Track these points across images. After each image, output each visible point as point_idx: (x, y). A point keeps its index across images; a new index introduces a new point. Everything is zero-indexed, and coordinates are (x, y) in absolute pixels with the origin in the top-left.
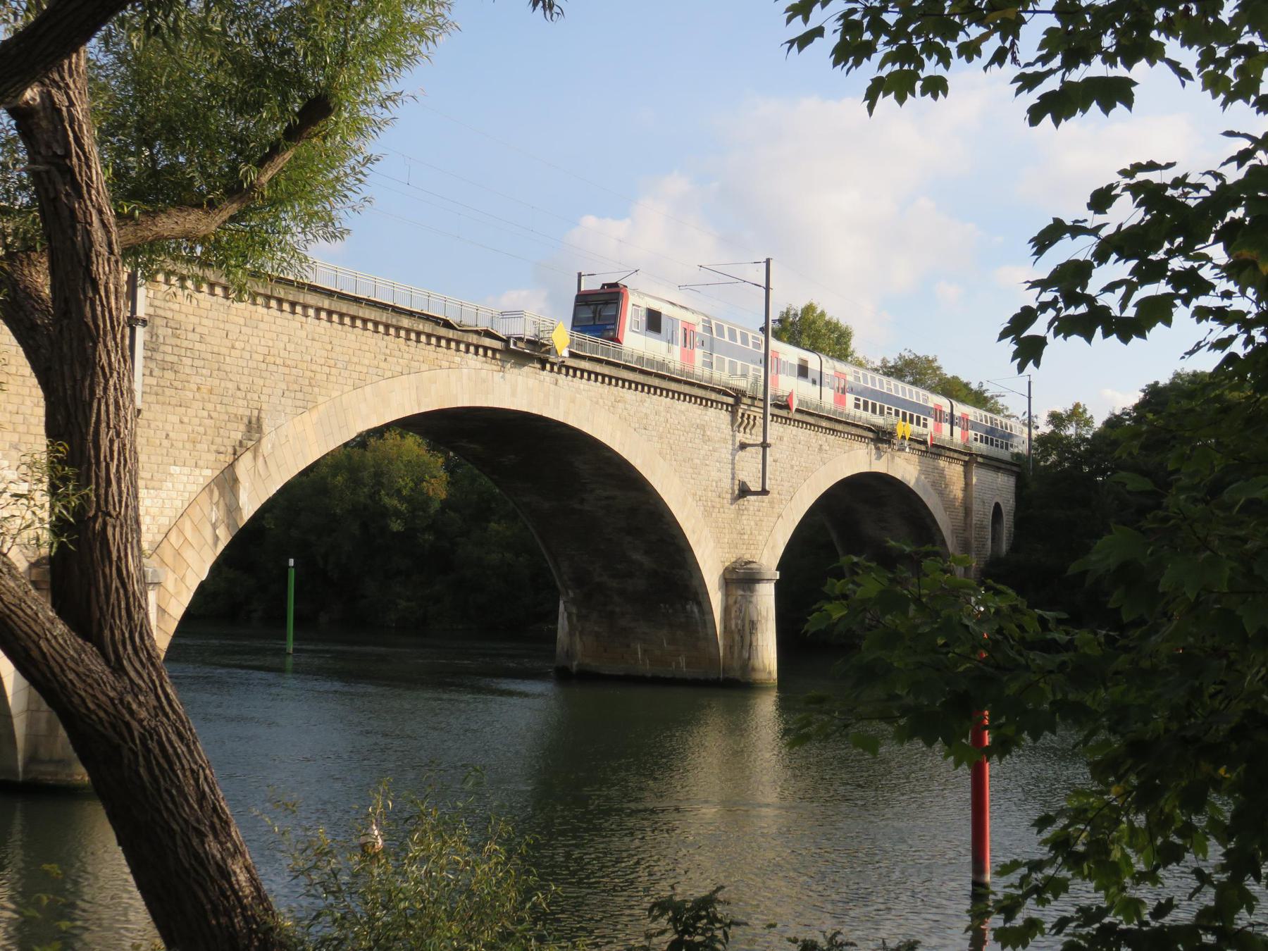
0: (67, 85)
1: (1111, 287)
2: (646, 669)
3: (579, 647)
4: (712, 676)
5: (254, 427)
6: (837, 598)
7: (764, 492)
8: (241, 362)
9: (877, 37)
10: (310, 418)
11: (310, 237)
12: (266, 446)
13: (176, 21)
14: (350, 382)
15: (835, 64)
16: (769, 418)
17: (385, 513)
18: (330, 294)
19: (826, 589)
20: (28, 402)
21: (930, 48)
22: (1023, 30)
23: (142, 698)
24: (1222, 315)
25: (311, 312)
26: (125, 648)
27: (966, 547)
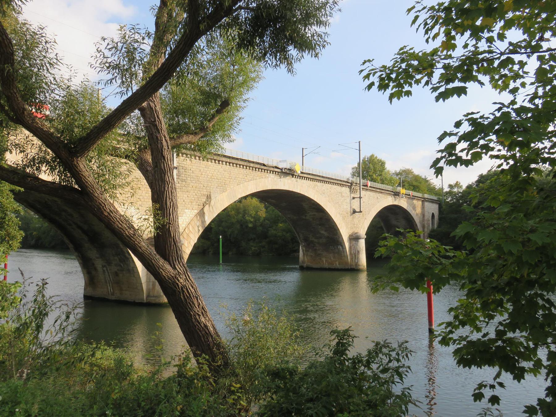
0: (154, 101)
1: (462, 151)
2: (326, 266)
3: (306, 259)
4: (347, 267)
5: (209, 197)
6: (383, 246)
7: (361, 212)
8: (205, 179)
9: (389, 82)
10: (225, 194)
11: (224, 141)
12: (212, 202)
13: (185, 82)
14: (236, 183)
15: (379, 91)
16: (361, 189)
17: (247, 222)
18: (229, 157)
19: (379, 244)
20: (144, 193)
21: (406, 83)
22: (434, 74)
23: (181, 276)
24: (497, 157)
25: (224, 163)
26: (176, 262)
27: (423, 227)
